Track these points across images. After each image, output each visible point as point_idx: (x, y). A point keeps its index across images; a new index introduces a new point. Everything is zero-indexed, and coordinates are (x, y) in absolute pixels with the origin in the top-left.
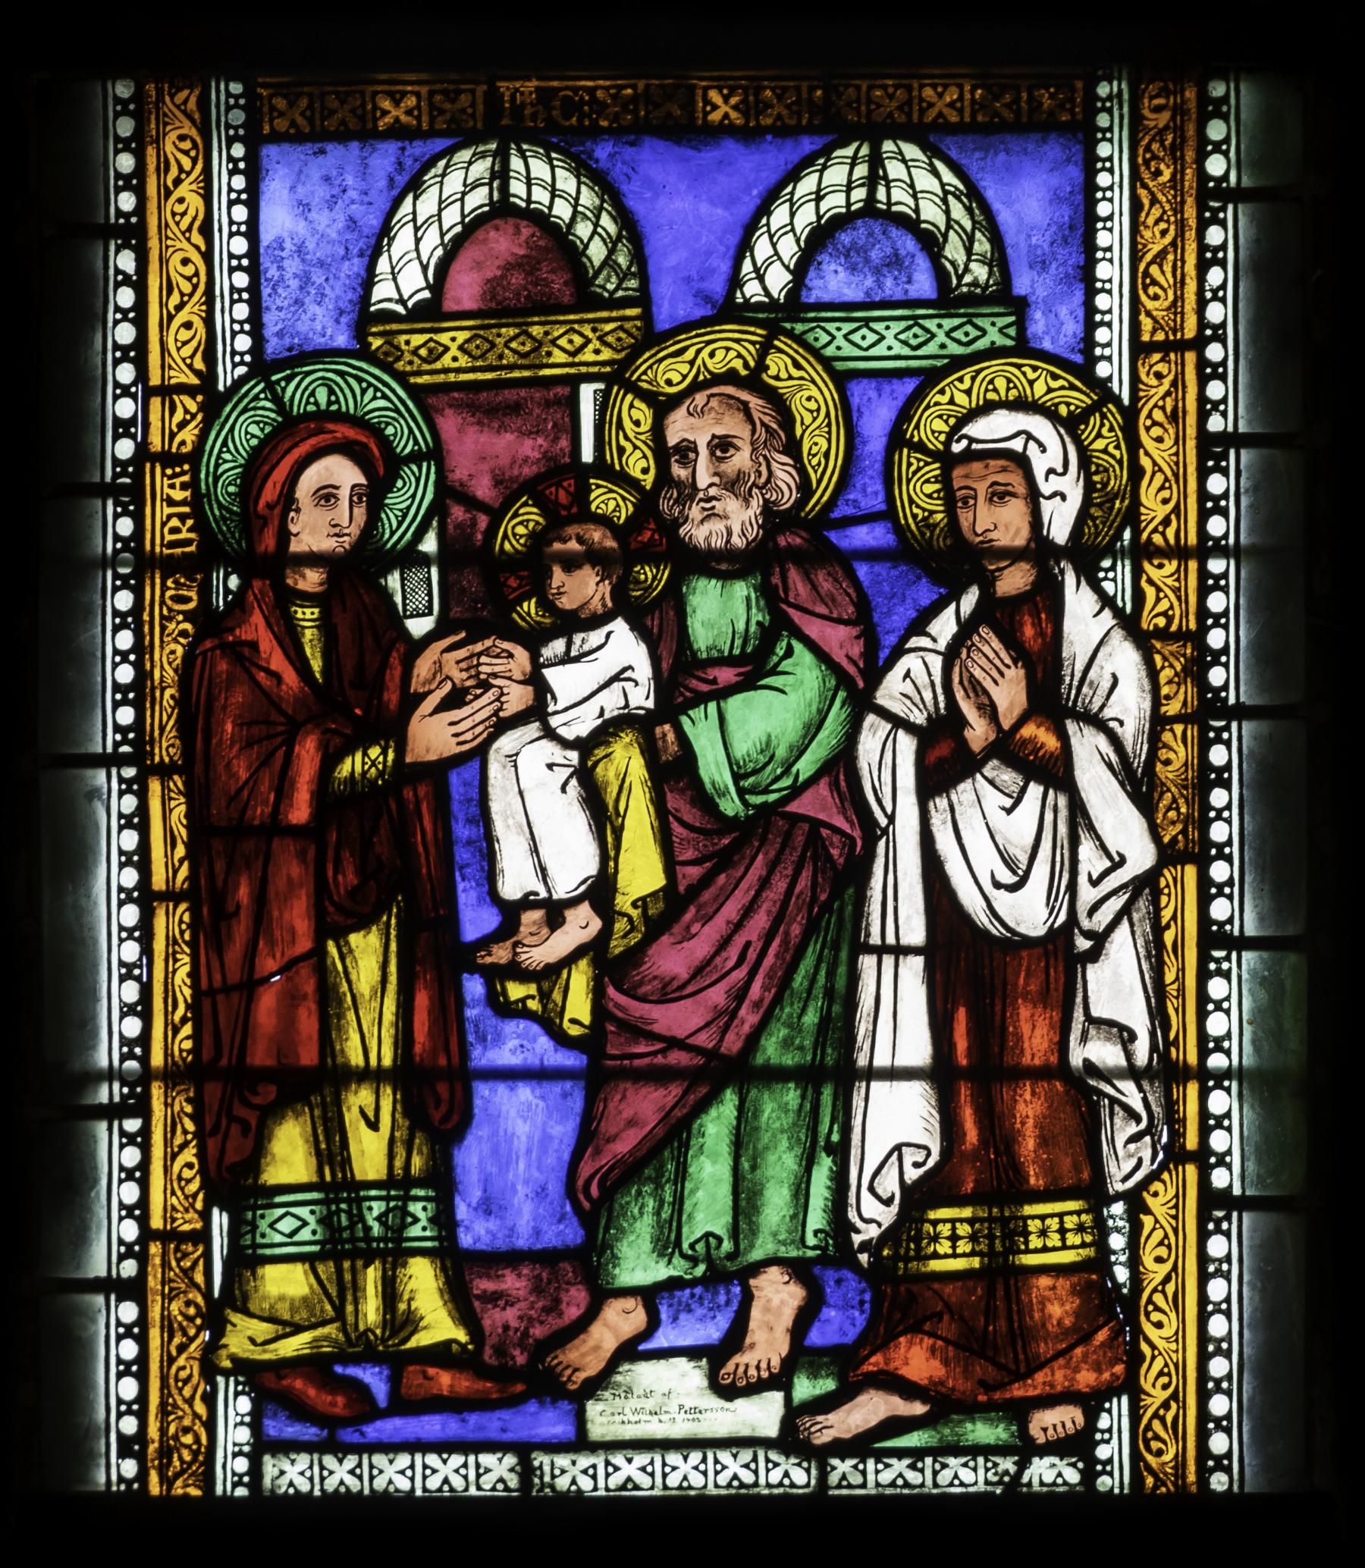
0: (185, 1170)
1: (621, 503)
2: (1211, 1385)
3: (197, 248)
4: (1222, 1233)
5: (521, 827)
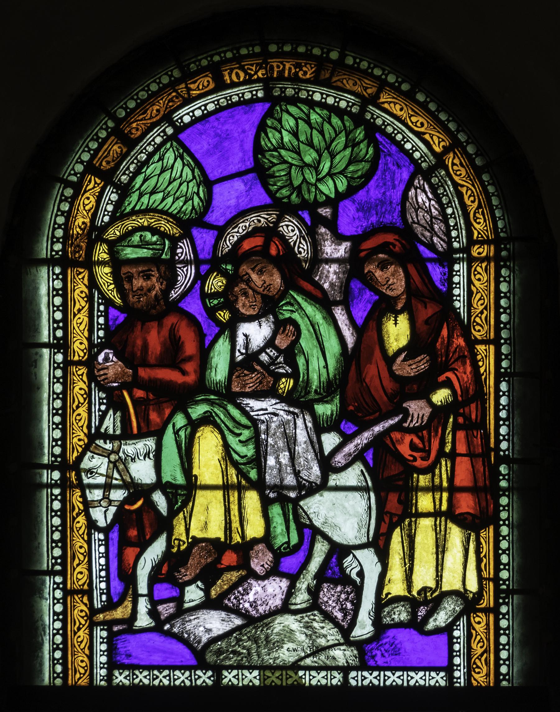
0: (79, 574)
1: (259, 218)
2: (61, 632)
3: (474, 286)
4: (505, 619)
5: (217, 466)
